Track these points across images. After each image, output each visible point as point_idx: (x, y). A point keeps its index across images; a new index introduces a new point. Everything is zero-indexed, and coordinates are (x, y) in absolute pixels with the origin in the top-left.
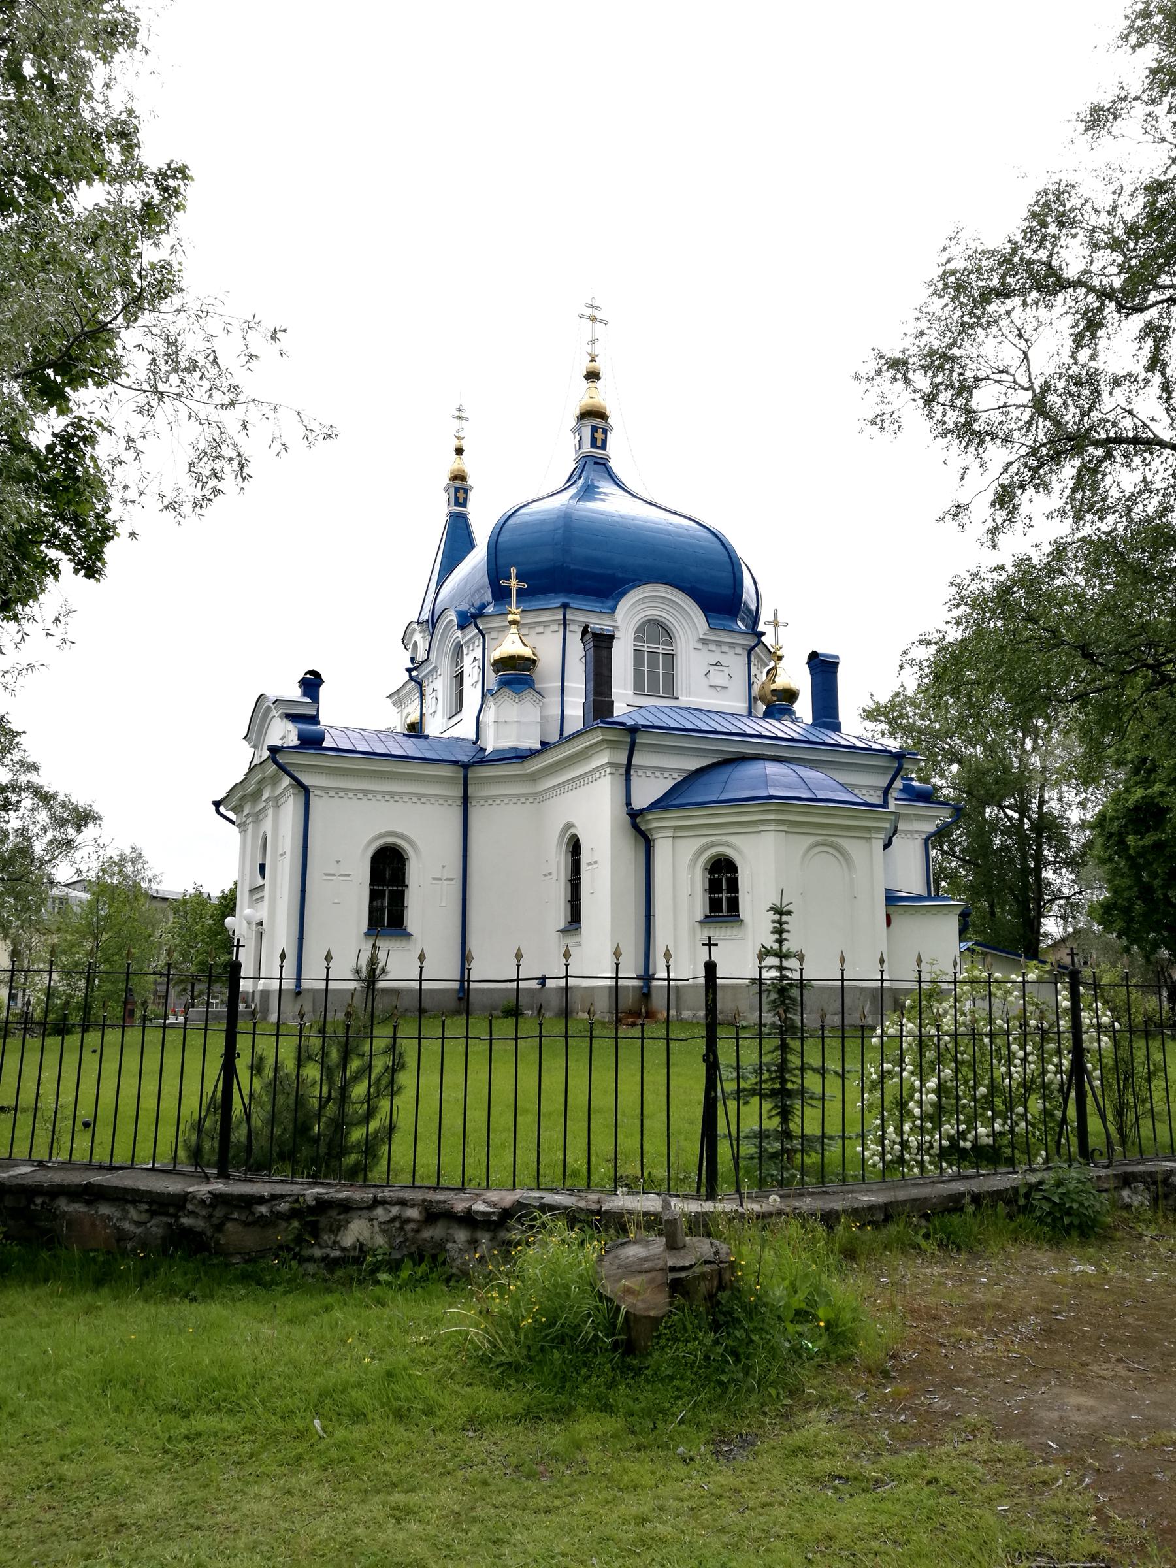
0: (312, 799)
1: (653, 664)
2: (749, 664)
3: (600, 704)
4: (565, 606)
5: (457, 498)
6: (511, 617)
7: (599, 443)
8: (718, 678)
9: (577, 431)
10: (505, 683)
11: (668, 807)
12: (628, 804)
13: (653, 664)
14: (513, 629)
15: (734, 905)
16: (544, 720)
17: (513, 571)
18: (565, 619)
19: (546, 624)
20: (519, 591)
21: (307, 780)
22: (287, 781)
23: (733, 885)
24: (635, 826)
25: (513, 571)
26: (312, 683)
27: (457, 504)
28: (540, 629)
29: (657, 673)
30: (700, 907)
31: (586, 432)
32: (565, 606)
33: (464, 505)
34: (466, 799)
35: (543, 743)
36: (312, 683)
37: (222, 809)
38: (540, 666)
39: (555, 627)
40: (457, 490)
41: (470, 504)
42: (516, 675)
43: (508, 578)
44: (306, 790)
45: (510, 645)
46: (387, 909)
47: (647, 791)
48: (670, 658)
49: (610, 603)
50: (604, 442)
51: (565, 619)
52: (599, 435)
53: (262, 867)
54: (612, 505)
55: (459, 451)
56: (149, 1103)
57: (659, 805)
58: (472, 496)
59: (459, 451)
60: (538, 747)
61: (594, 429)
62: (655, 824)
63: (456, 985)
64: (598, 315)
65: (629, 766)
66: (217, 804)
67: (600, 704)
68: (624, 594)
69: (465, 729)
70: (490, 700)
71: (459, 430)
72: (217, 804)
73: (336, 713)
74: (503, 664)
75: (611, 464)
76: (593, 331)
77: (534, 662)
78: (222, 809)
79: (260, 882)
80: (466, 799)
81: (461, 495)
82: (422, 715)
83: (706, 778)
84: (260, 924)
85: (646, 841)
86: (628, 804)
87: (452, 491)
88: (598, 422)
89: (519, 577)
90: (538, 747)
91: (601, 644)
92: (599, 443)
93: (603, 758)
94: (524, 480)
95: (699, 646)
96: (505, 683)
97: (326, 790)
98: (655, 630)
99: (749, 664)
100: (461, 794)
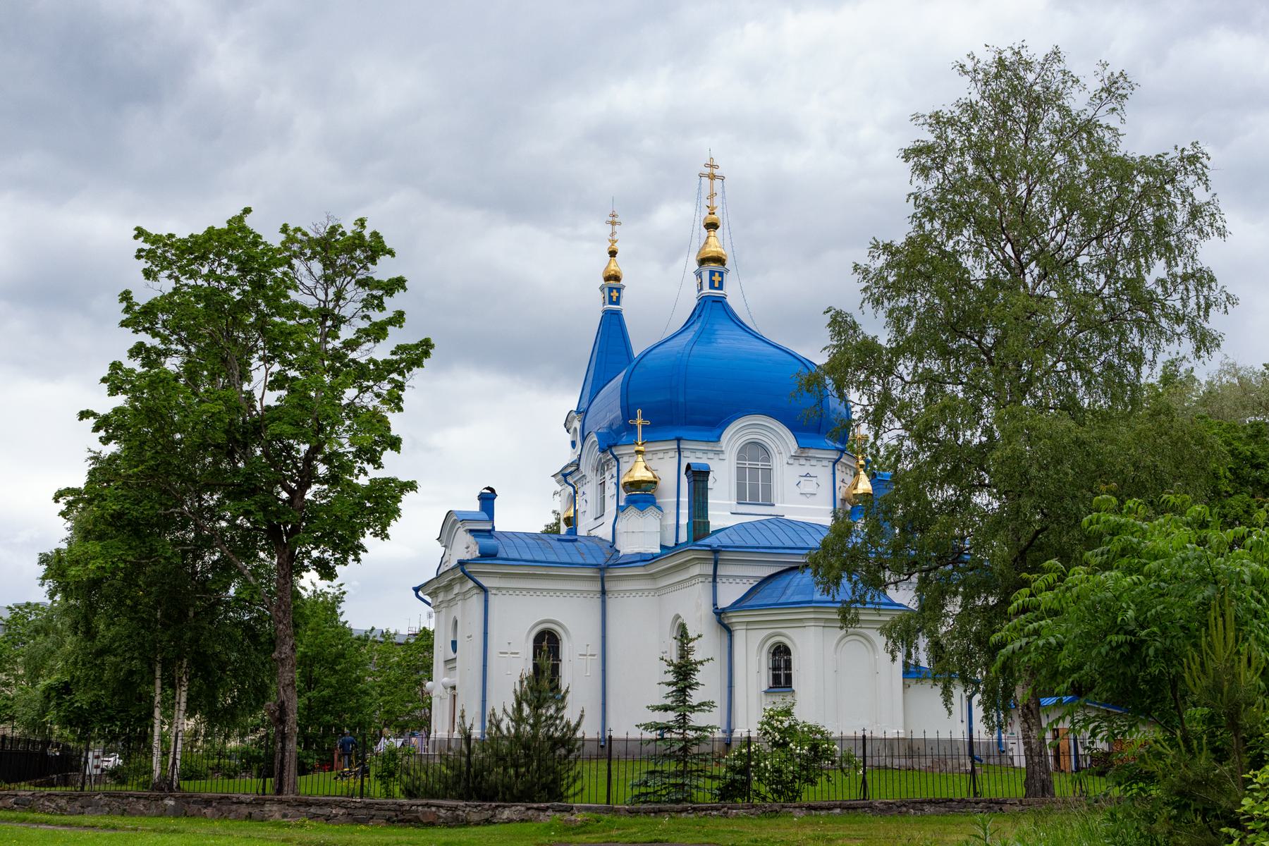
0: (491, 598)
1: (754, 478)
2: (834, 474)
3: (699, 526)
4: (679, 440)
5: (611, 297)
6: (637, 448)
7: (717, 285)
8: (808, 486)
9: (699, 275)
10: (631, 501)
11: (743, 609)
12: (715, 604)
13: (754, 478)
14: (640, 458)
15: (789, 678)
16: (663, 528)
17: (639, 412)
18: (679, 448)
19: (665, 451)
20: (643, 426)
21: (486, 582)
22: (471, 584)
23: (788, 665)
24: (720, 622)
25: (639, 412)
26: (487, 499)
27: (611, 302)
28: (660, 455)
29: (754, 488)
30: (765, 680)
31: (706, 276)
32: (679, 440)
33: (617, 303)
34: (604, 592)
35: (662, 547)
36: (487, 499)
37: (420, 593)
38: (661, 484)
39: (672, 454)
40: (611, 289)
41: (623, 301)
42: (641, 495)
43: (635, 417)
44: (484, 590)
45: (640, 474)
46: (781, 657)
47: (729, 594)
48: (768, 472)
49: (716, 432)
50: (721, 283)
51: (679, 448)
52: (717, 278)
53: (454, 643)
54: (727, 342)
55: (613, 253)
56: (896, 784)
57: (738, 605)
58: (624, 293)
59: (613, 253)
60: (658, 550)
61: (712, 273)
62: (734, 620)
63: (589, 730)
64: (716, 172)
65: (715, 576)
66: (416, 590)
67: (699, 526)
68: (728, 423)
69: (604, 532)
70: (621, 515)
71: (612, 234)
72: (416, 590)
73: (506, 520)
74: (634, 485)
75: (729, 301)
76: (712, 188)
77: (655, 483)
78: (420, 593)
79: (453, 656)
80: (604, 592)
81: (615, 294)
82: (576, 511)
83: (774, 584)
84: (454, 688)
85: (728, 630)
86: (715, 604)
87: (606, 290)
88: (713, 266)
89: (644, 417)
90: (658, 550)
91: (698, 478)
92: (717, 285)
93: (696, 570)
94: (659, 305)
95: (791, 461)
96: (631, 501)
97: (498, 589)
98: (755, 450)
99: (834, 474)
100: (599, 588)
